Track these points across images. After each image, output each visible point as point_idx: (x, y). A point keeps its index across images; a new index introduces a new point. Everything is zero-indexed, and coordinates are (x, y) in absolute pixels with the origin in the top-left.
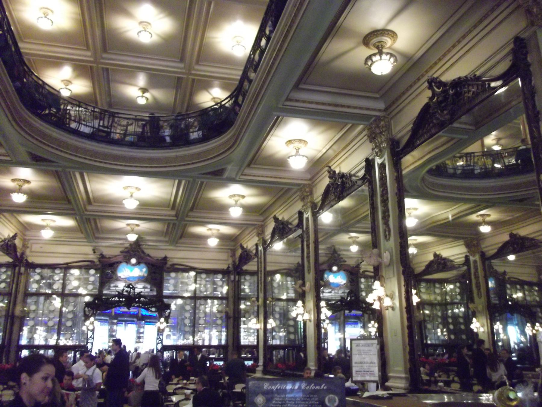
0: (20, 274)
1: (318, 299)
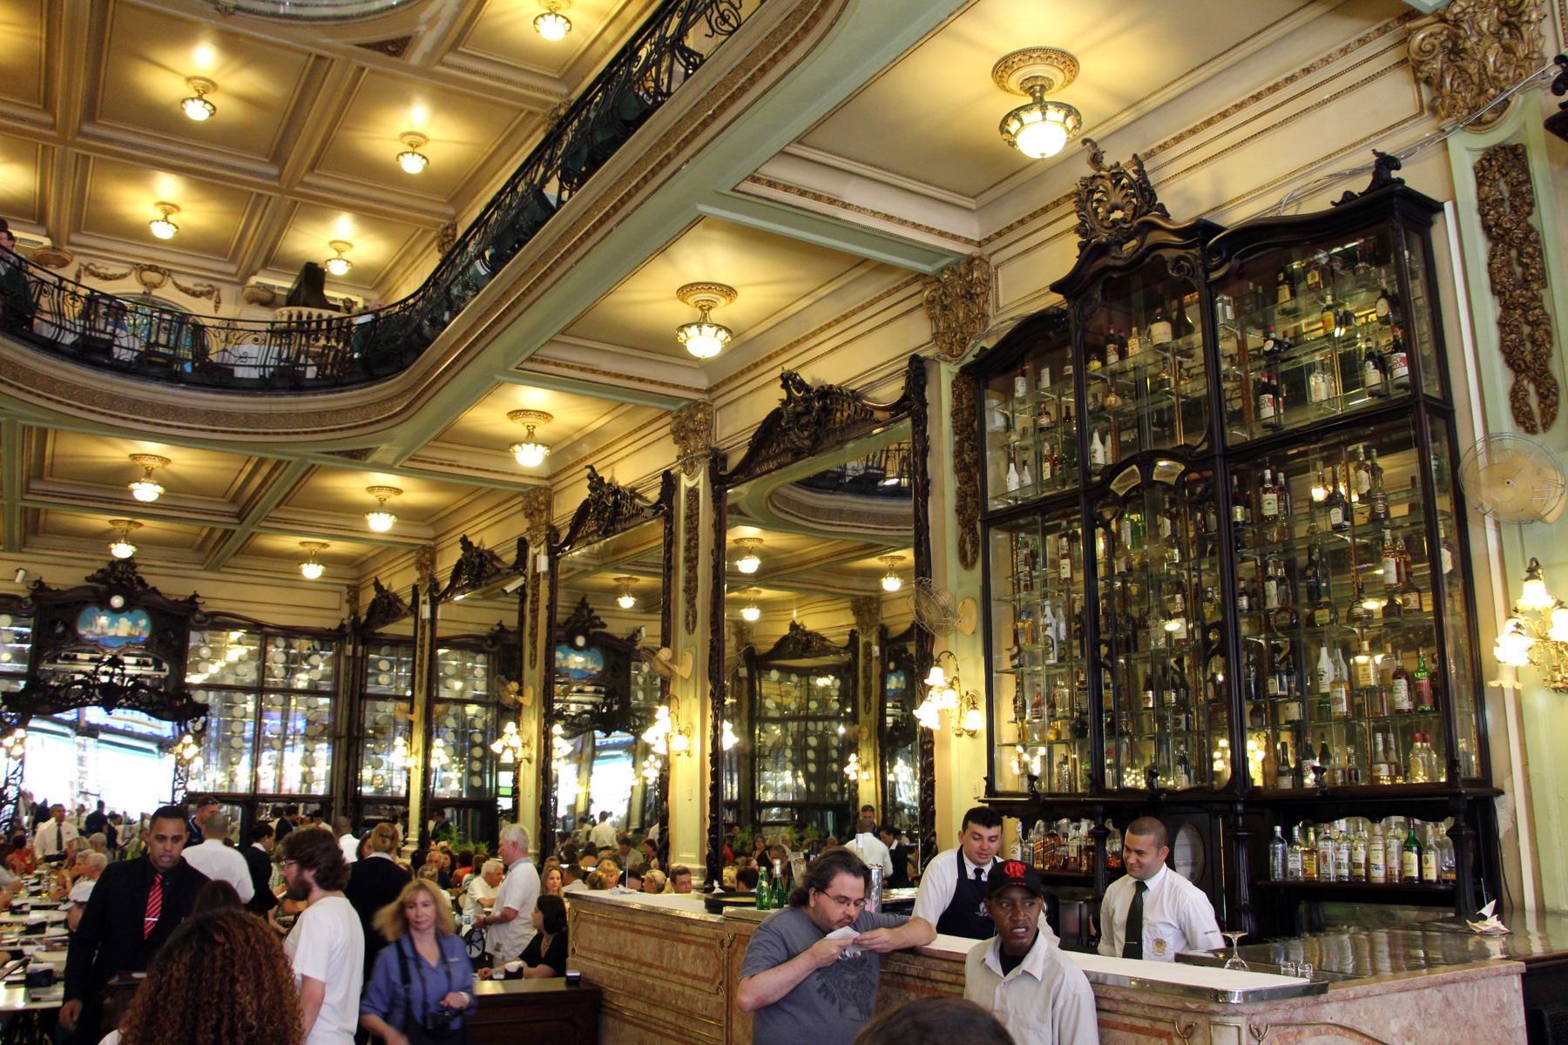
1: (550, 717)
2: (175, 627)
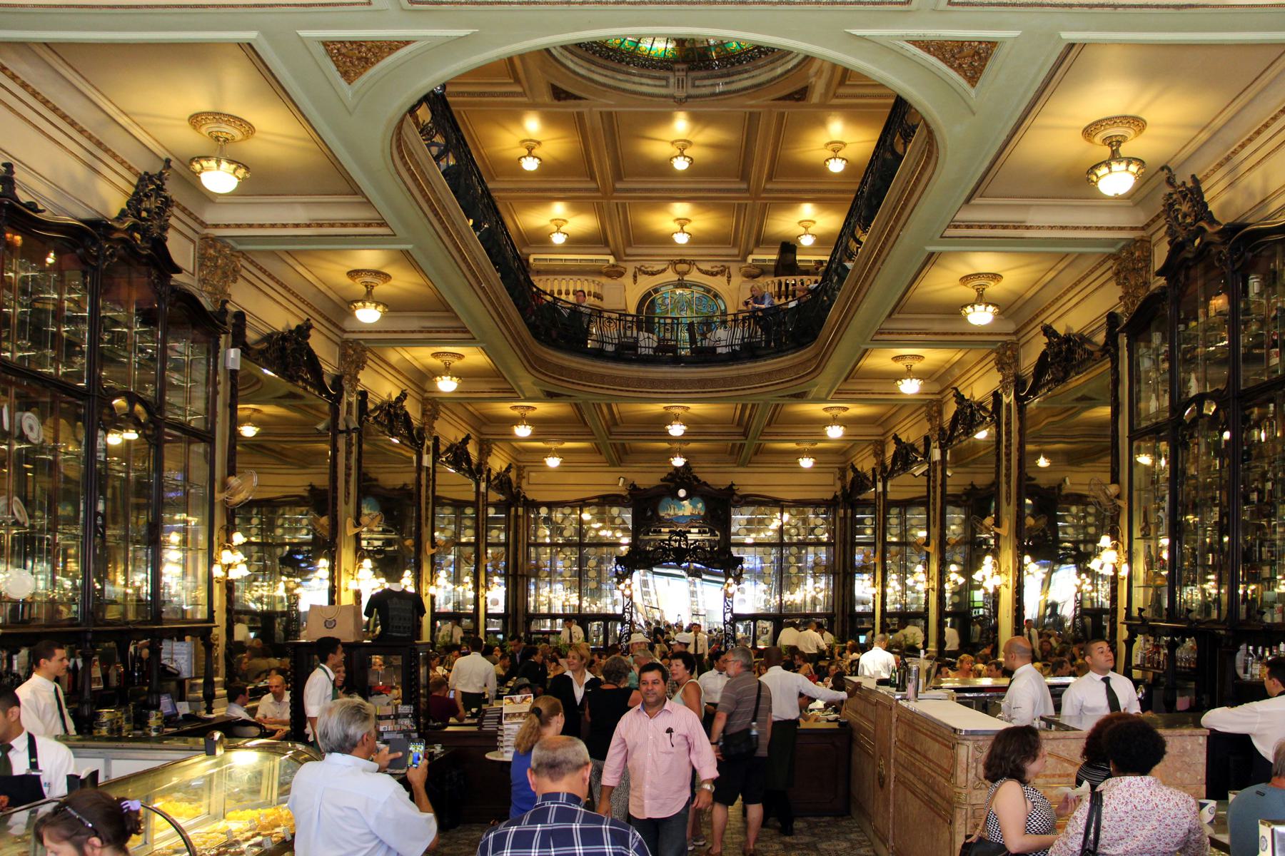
0: (517, 516)
2: (720, 505)
